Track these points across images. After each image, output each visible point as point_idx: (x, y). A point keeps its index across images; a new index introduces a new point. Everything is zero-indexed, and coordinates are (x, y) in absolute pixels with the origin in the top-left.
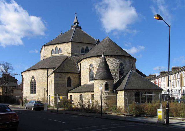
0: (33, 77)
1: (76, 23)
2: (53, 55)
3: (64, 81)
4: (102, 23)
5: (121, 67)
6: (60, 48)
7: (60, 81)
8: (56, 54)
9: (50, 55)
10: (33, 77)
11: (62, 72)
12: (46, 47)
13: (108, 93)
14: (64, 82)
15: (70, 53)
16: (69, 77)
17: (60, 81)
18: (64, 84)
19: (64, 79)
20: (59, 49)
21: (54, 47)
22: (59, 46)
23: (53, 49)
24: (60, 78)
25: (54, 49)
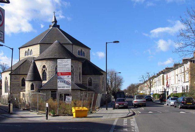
0: (44, 67)
1: (54, 22)
2: (26, 56)
3: (18, 81)
4: (129, 87)
5: (44, 69)
6: (31, 50)
7: (15, 81)
8: (29, 56)
9: (24, 57)
10: (44, 67)
11: (16, 74)
12: (21, 49)
13: (33, 92)
14: (18, 83)
15: (39, 54)
16: (23, 78)
17: (15, 81)
18: (18, 84)
19: (18, 80)
20: (30, 50)
21: (26, 49)
22: (30, 48)
23: (26, 51)
24: (15, 79)
25: (27, 51)
